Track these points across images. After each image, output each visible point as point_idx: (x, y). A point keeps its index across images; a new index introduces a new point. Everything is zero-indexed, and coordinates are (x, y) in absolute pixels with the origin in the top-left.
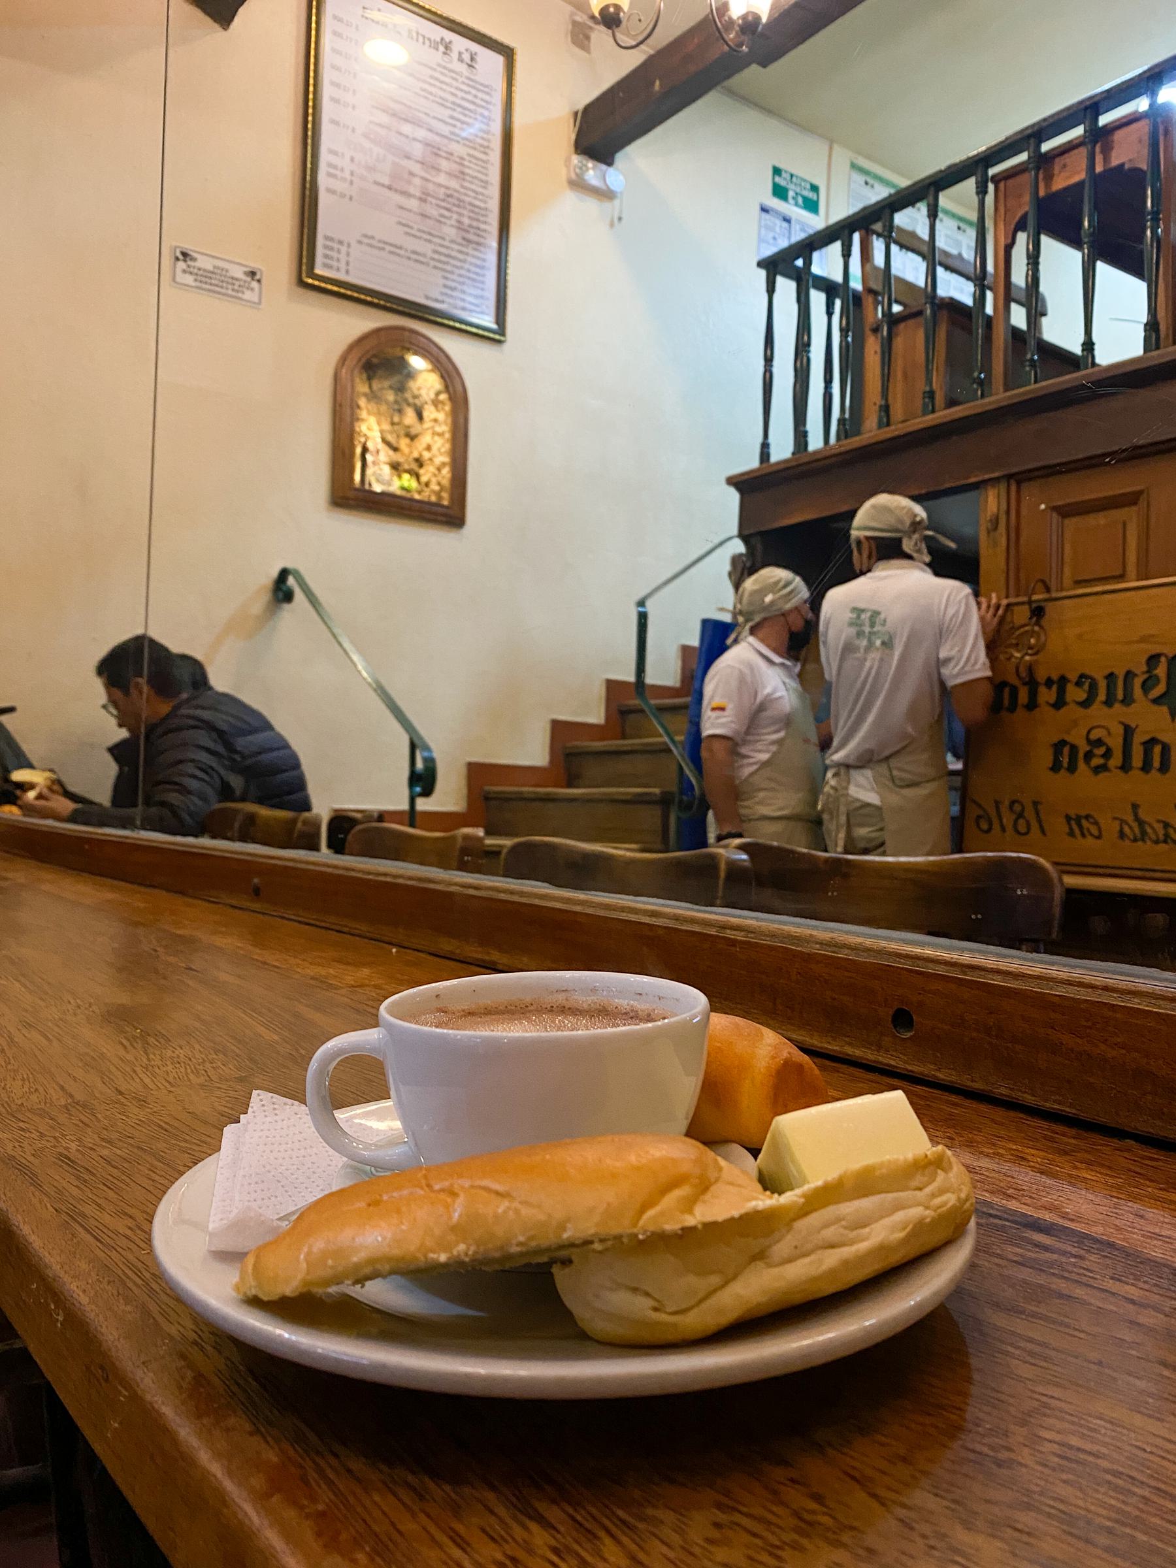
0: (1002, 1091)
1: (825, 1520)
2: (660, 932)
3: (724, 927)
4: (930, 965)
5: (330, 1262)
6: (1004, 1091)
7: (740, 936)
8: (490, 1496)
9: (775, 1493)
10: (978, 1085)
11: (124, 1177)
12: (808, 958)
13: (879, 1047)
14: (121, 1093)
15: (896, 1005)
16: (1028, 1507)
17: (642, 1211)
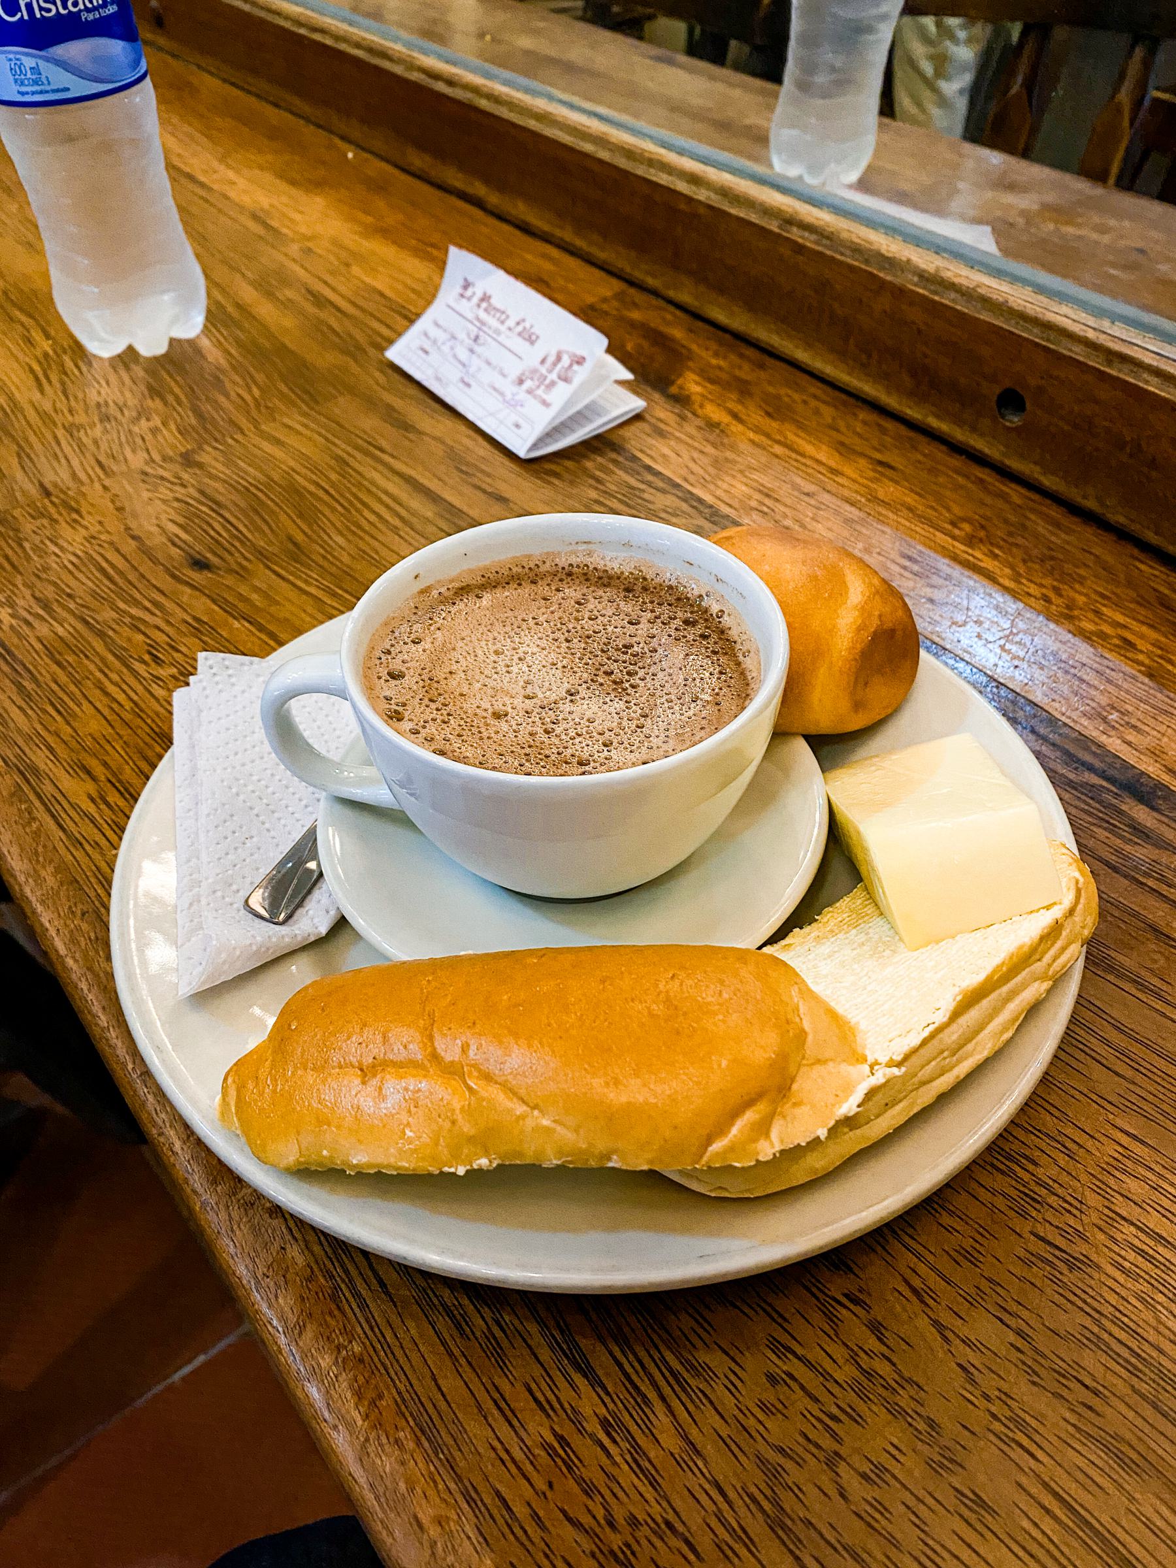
0: (1118, 518)
1: (884, 1368)
2: (702, 211)
3: (790, 221)
4: (1065, 341)
5: (325, 1153)
6: (1122, 519)
7: (808, 241)
8: (533, 1328)
9: (830, 1317)
10: (1091, 504)
11: (72, 688)
12: (900, 293)
13: (974, 429)
14: (48, 494)
15: (1008, 383)
16: (1097, 1343)
17: (709, 1141)
